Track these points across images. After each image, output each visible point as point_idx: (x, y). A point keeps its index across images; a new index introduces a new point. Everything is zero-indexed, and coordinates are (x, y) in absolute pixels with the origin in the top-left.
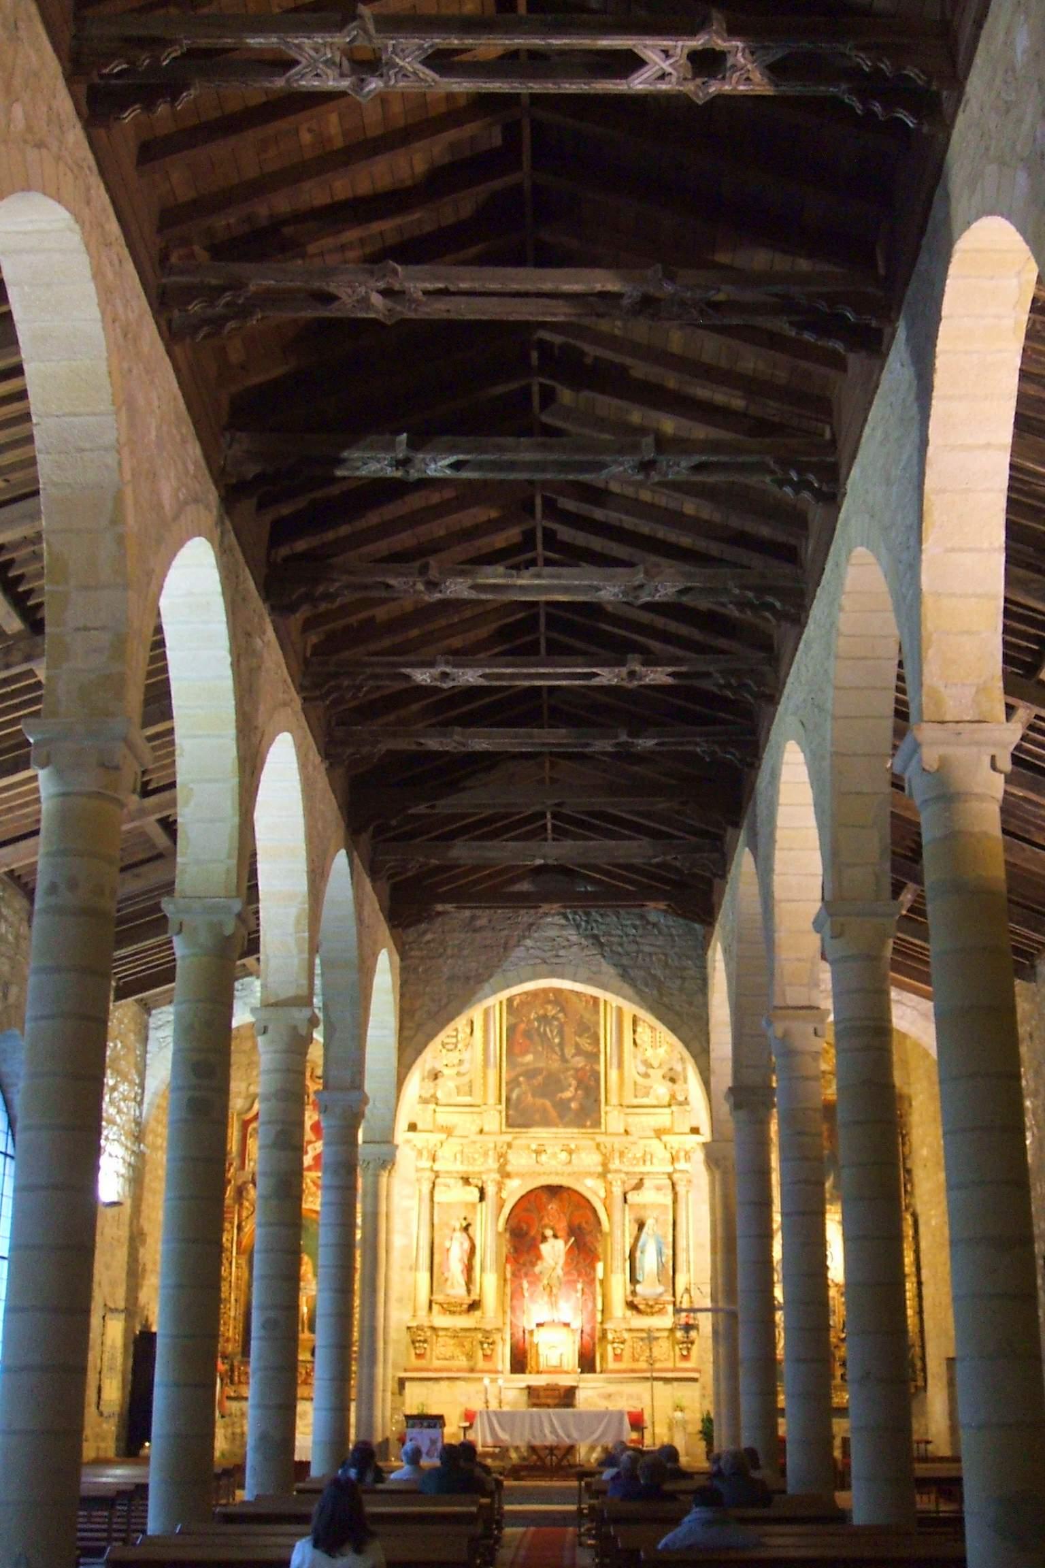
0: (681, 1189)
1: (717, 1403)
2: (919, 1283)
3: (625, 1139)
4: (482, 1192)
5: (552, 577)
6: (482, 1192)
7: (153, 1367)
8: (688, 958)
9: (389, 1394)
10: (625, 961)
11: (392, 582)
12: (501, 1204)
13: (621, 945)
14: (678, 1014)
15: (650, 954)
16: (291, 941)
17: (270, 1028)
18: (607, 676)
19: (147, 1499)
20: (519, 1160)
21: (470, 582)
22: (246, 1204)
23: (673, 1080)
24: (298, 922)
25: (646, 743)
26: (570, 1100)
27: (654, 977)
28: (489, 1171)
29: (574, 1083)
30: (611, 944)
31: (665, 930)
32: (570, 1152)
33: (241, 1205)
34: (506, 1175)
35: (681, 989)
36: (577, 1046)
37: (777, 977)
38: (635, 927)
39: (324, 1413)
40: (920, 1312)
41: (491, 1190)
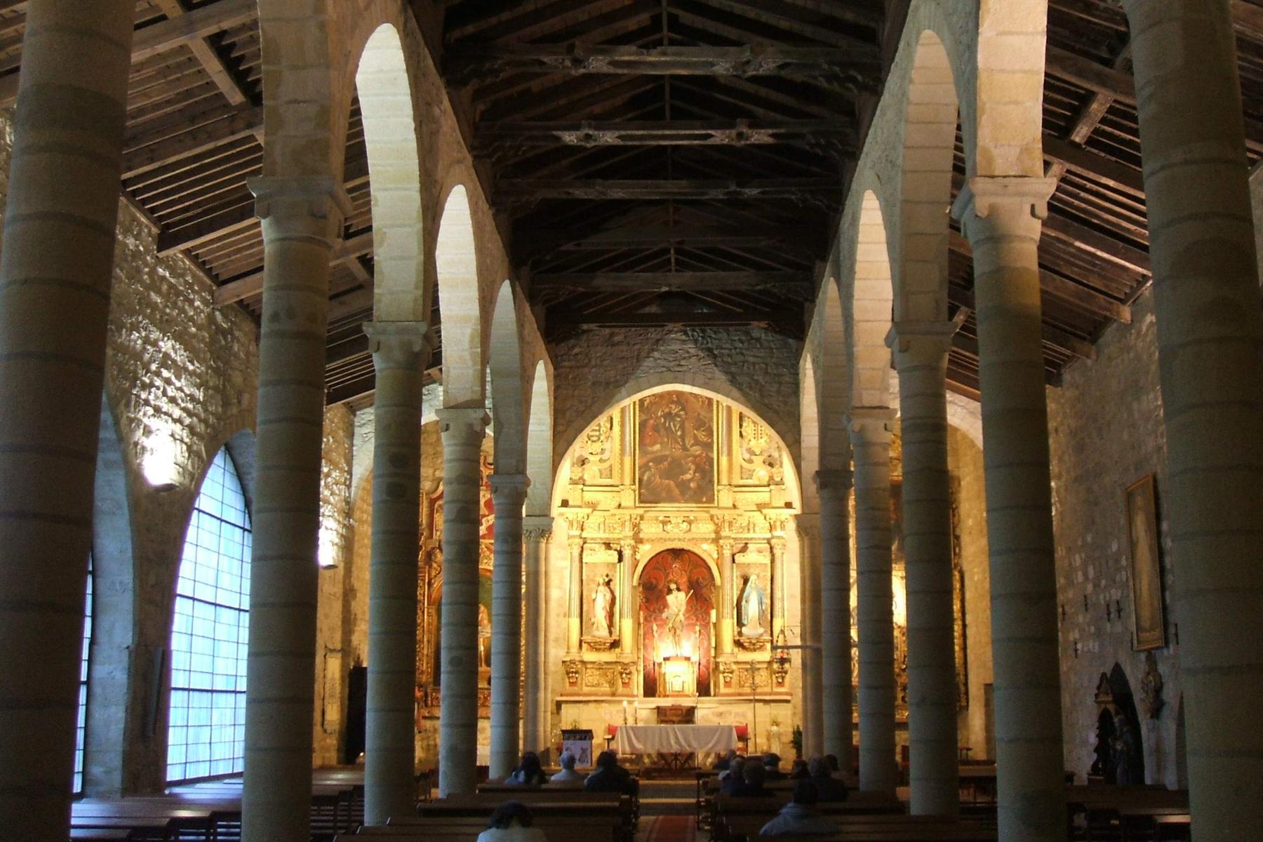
0: (777, 552)
2: (964, 626)
3: (733, 511)
5: (675, 54)
15: (754, 364)
16: (467, 355)
17: (451, 425)
18: (719, 137)
21: (608, 59)
22: (435, 565)
23: (771, 465)
24: (471, 341)
25: (751, 192)
26: (690, 481)
27: (757, 382)
29: (693, 467)
32: (690, 523)
33: (431, 566)
36: (695, 437)
37: (856, 383)
38: (742, 342)
40: (964, 648)
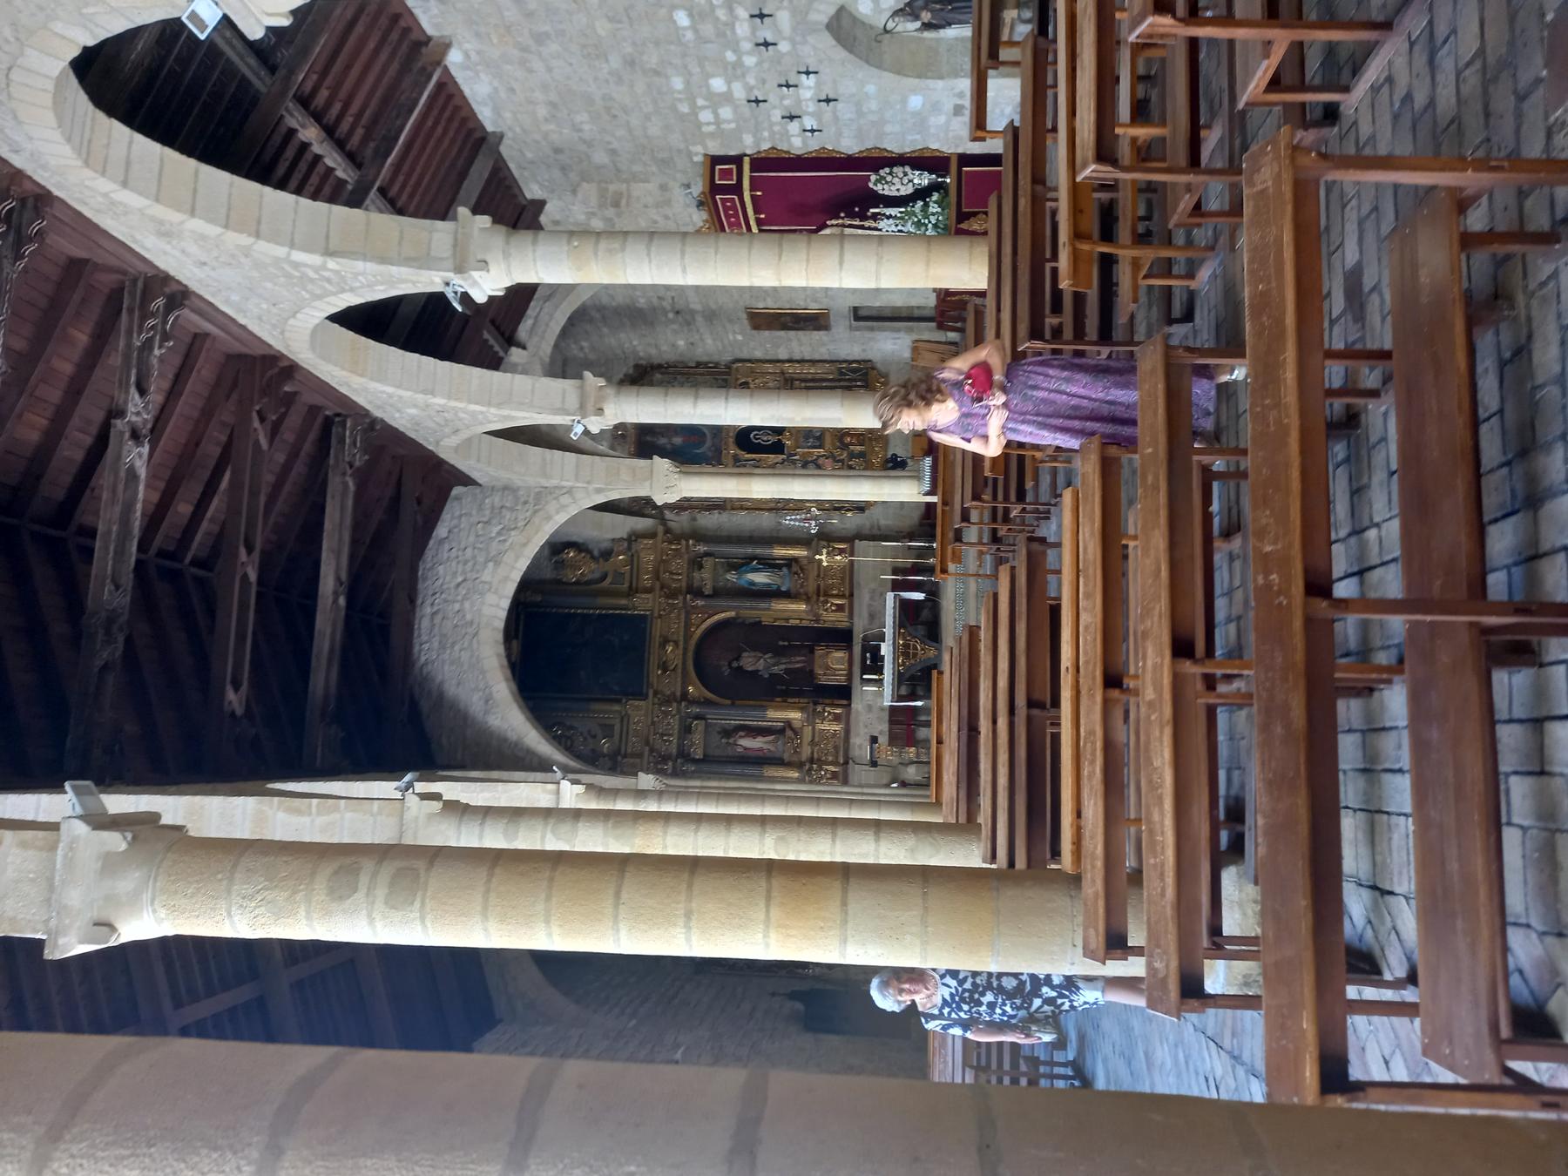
1: (1023, 114)
4: (698, 717)
6: (698, 717)
7: (320, 548)
8: (483, 502)
9: (846, 789)
10: (481, 559)
11: (99, 663)
12: (708, 703)
13: (466, 563)
14: (536, 512)
19: (717, 430)
20: (671, 685)
27: (499, 534)
28: (679, 711)
30: (464, 572)
31: (455, 522)
34: (685, 696)
35: (512, 509)
39: (688, 249)
41: (696, 710)
